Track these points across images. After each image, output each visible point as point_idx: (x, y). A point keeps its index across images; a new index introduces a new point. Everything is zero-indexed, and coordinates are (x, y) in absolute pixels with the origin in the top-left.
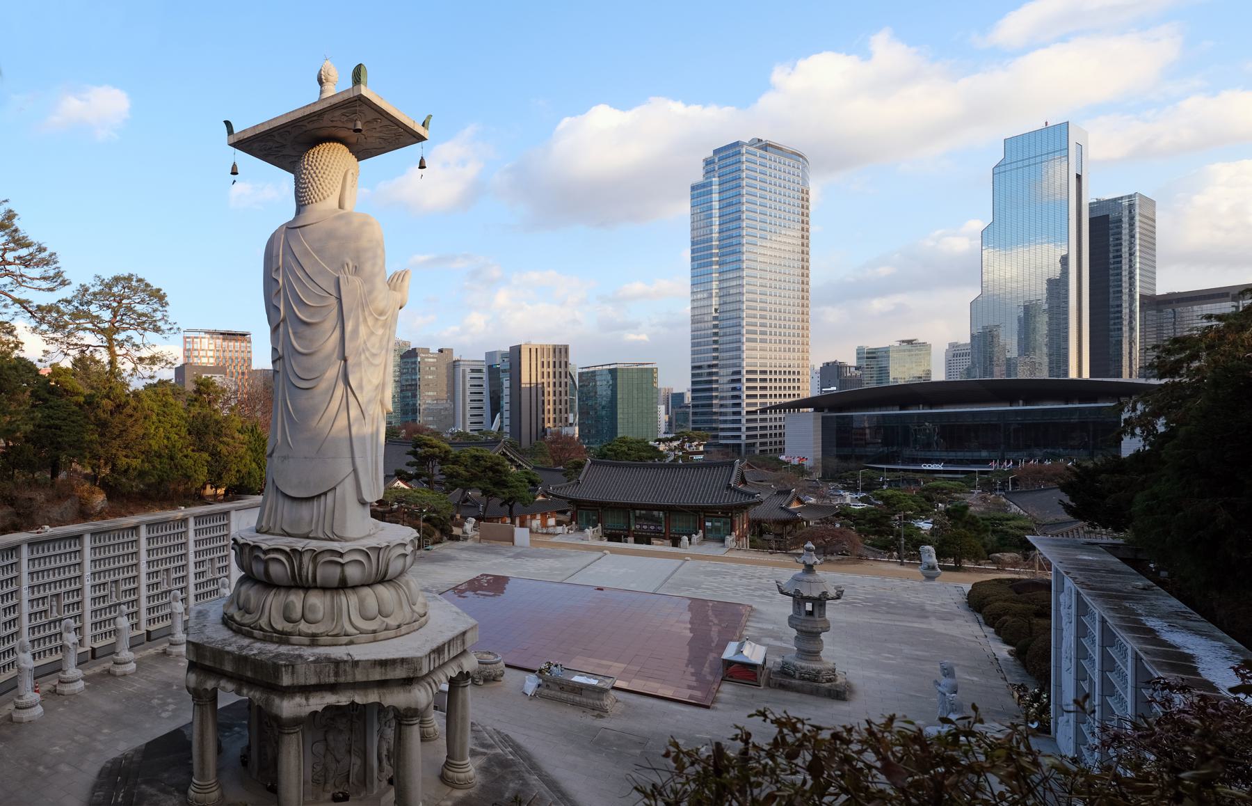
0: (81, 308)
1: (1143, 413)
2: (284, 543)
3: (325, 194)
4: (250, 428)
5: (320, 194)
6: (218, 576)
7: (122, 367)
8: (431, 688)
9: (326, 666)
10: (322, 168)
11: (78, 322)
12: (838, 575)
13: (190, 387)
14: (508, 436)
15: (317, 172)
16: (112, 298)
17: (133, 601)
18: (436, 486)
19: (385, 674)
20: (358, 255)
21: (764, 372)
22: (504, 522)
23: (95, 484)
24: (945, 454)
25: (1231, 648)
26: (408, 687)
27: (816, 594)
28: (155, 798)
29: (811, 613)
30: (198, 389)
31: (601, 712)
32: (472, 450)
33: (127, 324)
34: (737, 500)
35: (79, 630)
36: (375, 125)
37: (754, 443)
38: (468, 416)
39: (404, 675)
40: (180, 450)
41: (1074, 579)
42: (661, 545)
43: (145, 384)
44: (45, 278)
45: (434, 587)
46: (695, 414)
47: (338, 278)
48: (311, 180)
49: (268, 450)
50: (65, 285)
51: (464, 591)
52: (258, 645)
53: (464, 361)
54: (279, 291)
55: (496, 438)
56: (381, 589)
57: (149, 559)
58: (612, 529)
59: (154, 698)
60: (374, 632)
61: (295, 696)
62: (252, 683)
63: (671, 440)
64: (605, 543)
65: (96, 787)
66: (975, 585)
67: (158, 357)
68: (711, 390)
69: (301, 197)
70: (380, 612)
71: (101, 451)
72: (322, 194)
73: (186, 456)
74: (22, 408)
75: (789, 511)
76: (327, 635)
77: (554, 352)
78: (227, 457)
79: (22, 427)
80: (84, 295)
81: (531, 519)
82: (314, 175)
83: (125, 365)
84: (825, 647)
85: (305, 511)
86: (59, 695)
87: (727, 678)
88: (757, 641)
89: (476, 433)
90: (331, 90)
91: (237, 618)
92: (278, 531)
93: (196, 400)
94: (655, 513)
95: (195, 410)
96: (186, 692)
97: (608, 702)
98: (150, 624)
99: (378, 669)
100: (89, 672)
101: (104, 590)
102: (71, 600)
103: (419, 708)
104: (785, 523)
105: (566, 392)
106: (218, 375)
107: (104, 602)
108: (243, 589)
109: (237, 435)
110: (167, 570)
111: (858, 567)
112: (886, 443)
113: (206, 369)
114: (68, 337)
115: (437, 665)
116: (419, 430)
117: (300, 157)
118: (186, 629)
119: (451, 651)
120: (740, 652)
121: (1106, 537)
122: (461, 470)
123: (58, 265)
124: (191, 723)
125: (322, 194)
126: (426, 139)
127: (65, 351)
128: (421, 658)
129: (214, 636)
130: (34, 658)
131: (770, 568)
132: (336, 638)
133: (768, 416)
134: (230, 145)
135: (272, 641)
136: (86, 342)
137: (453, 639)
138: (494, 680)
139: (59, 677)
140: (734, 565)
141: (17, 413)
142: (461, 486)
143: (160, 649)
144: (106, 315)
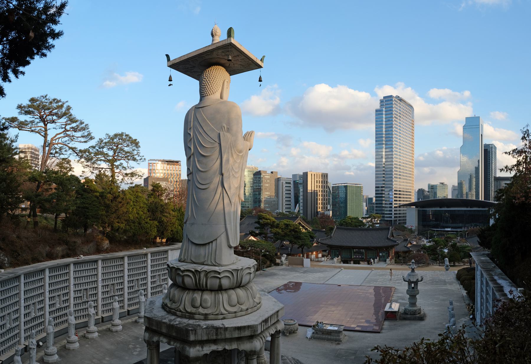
0: (99, 150)
1: (494, 212)
2: (192, 267)
5: (211, 91)
6: (162, 283)
10: (212, 78)
11: (97, 157)
12: (422, 272)
13: (150, 188)
14: (302, 215)
15: (210, 80)
17: (121, 295)
20: (229, 123)
21: (400, 191)
24: (451, 225)
25: (510, 283)
26: (251, 340)
27: (415, 280)
29: (413, 288)
30: (153, 189)
32: (285, 221)
33: (120, 157)
34: (391, 244)
35: (96, 307)
37: (397, 220)
38: (284, 204)
40: (144, 220)
41: (480, 266)
44: (83, 137)
45: (266, 289)
47: (219, 134)
48: (207, 84)
49: (185, 221)
50: (92, 139)
52: (179, 319)
53: (283, 178)
54: (191, 139)
55: (297, 215)
57: (129, 274)
58: (346, 258)
59: (131, 344)
60: (235, 312)
61: (197, 346)
62: (175, 339)
63: (368, 218)
66: (458, 271)
67: (135, 173)
68: (382, 197)
70: (238, 302)
71: (106, 220)
72: (212, 91)
73: (146, 223)
74: (71, 199)
75: (408, 248)
76: (213, 315)
77: (322, 176)
78: (166, 223)
79: (71, 208)
80: (101, 144)
81: (311, 254)
82: (209, 82)
83: (119, 177)
86: (86, 338)
87: (386, 319)
88: (396, 301)
89: (287, 213)
90: (218, 39)
91: (169, 305)
93: (152, 194)
94: (362, 250)
95: (152, 199)
99: (237, 332)
100: (100, 329)
102: (92, 292)
103: (256, 350)
104: (405, 252)
105: (327, 195)
106: (164, 182)
107: (107, 294)
108: (172, 290)
109: (171, 212)
110: (137, 280)
111: (426, 268)
112: (436, 221)
113: (158, 179)
114: (93, 164)
115: (265, 328)
116: (261, 211)
117: (202, 72)
119: (272, 321)
120: (390, 307)
121: (487, 252)
122: (280, 231)
123: (89, 130)
125: (212, 91)
126: (262, 67)
127: (92, 171)
128: (257, 325)
129: (157, 314)
130: (76, 319)
131: (401, 271)
132: (218, 316)
133: (401, 209)
134: (168, 66)
135: (186, 318)
136: (101, 167)
137: (273, 315)
138: (294, 333)
139: (87, 330)
141: (69, 201)
142: (280, 239)
144: (111, 153)
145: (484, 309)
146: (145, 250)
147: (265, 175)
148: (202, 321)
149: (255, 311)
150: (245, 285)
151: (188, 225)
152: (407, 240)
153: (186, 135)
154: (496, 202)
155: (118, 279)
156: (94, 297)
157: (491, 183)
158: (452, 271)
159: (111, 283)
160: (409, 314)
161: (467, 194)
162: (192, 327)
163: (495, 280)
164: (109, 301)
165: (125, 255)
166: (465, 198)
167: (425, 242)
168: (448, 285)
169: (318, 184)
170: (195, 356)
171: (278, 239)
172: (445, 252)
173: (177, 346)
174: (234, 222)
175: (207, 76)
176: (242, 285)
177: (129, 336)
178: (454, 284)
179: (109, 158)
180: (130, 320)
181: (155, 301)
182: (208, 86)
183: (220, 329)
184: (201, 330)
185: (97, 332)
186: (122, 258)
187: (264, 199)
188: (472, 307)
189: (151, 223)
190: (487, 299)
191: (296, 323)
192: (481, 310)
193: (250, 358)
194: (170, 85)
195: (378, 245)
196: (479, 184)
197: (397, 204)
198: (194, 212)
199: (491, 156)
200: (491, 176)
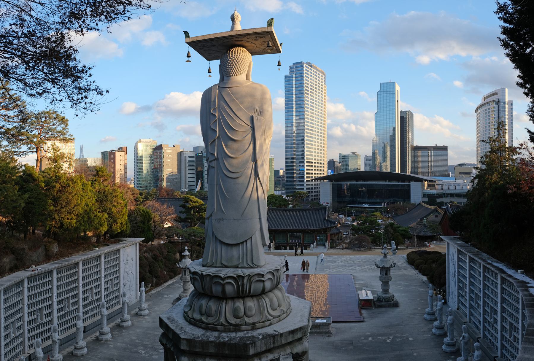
2: (230, 272)
3: (241, 72)
9: (269, 339)
19: (294, 337)
20: (261, 107)
21: (312, 162)
48: (235, 65)
72: (240, 72)
76: (260, 322)
84: (390, 288)
85: (235, 252)
94: (298, 234)
99: (291, 336)
131: (348, 256)
133: (313, 183)
140: (336, 256)
147: (167, 150)
151: (213, 221)
187: (166, 176)
198: (222, 205)
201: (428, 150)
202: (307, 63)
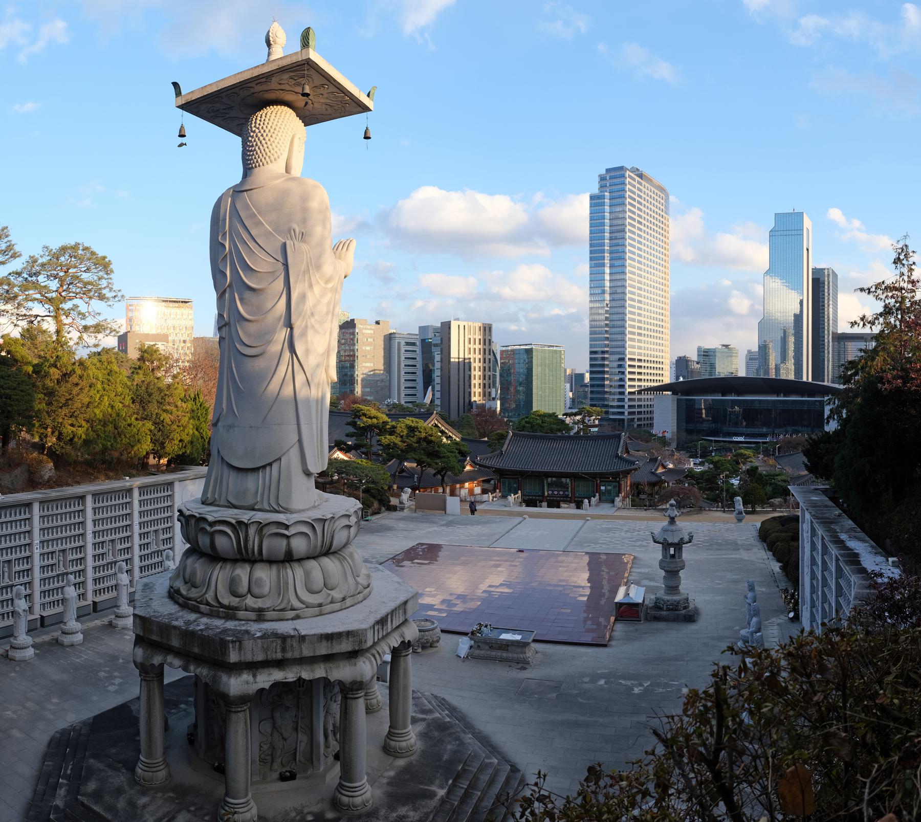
0: (30, 279)
2: (229, 515)
3: (272, 158)
4: (192, 396)
5: (267, 158)
6: (162, 548)
7: (69, 336)
8: (375, 659)
9: (273, 642)
10: (269, 131)
11: (27, 293)
13: (133, 354)
14: (439, 409)
15: (265, 135)
16: (59, 268)
17: (79, 571)
18: (374, 457)
21: (640, 360)
22: (436, 491)
23: (43, 453)
24: (745, 429)
25: (872, 547)
26: (353, 660)
27: (676, 540)
28: (103, 774)
29: (673, 556)
31: (523, 664)
34: (624, 467)
35: (29, 597)
36: (321, 91)
37: (634, 419)
39: (350, 649)
41: (810, 513)
42: (567, 508)
43: (89, 353)
46: (592, 392)
48: (259, 143)
51: (403, 560)
52: (205, 620)
55: (428, 410)
56: (325, 561)
57: (95, 530)
59: (101, 671)
60: (320, 605)
62: (199, 660)
63: (576, 414)
64: (524, 509)
65: (46, 757)
66: (763, 523)
69: (248, 160)
70: (325, 585)
72: (269, 157)
75: (656, 475)
76: (274, 610)
78: (170, 426)
81: (460, 488)
82: (261, 138)
85: (250, 482)
87: (619, 618)
88: (638, 583)
89: (410, 405)
90: (278, 53)
91: (184, 592)
92: (223, 502)
93: (140, 368)
94: (563, 480)
96: (133, 666)
97: (529, 654)
98: (96, 595)
99: (324, 643)
100: (38, 640)
101: (52, 558)
102: (22, 568)
103: (364, 680)
104: (652, 485)
105: (490, 367)
107: (52, 571)
108: (190, 561)
109: (179, 403)
110: (113, 541)
111: (696, 517)
112: (715, 420)
113: (147, 336)
114: (18, 308)
115: (380, 636)
116: (355, 402)
117: (247, 120)
118: (132, 602)
119: (394, 622)
122: (397, 440)
123: (9, 238)
124: (138, 698)
125: (269, 157)
127: (15, 322)
128: (366, 630)
129: (161, 610)
131: (645, 522)
133: (642, 397)
136: (34, 312)
137: (396, 609)
138: (431, 646)
139: (11, 642)
140: (621, 522)
143: (106, 621)
145: (818, 599)
146: (128, 481)
147: (363, 329)
148: (252, 623)
149: (359, 603)
150: (339, 550)
151: (221, 429)
152: (656, 459)
153: (216, 247)
154: (842, 387)
155: (72, 539)
156: (26, 577)
157: (826, 344)
158: (751, 523)
159: (60, 547)
160: (665, 608)
161: (777, 369)
162: (234, 635)
163: (842, 542)
164: (56, 583)
165: (88, 492)
166: (774, 377)
167: (693, 465)
168: (742, 550)
169: (472, 346)
170: (239, 693)
171: (391, 457)
172: (733, 484)
173: (202, 674)
174: (317, 424)
175: (257, 126)
176: (332, 550)
177: (98, 653)
178: (755, 550)
179: (51, 295)
180: (98, 623)
181: (154, 585)
182: (261, 147)
183: (289, 639)
184: (251, 641)
185: (33, 646)
186: (82, 498)
187: (362, 376)
188: (793, 596)
189: (139, 426)
190: (824, 578)
191: (436, 627)
192: (812, 601)
193: (351, 696)
194: (181, 145)
195: (597, 470)
196: (802, 347)
197: (634, 386)
198: (234, 403)
199: (826, 291)
200: (826, 332)
201: (866, 342)
202: (635, 170)
